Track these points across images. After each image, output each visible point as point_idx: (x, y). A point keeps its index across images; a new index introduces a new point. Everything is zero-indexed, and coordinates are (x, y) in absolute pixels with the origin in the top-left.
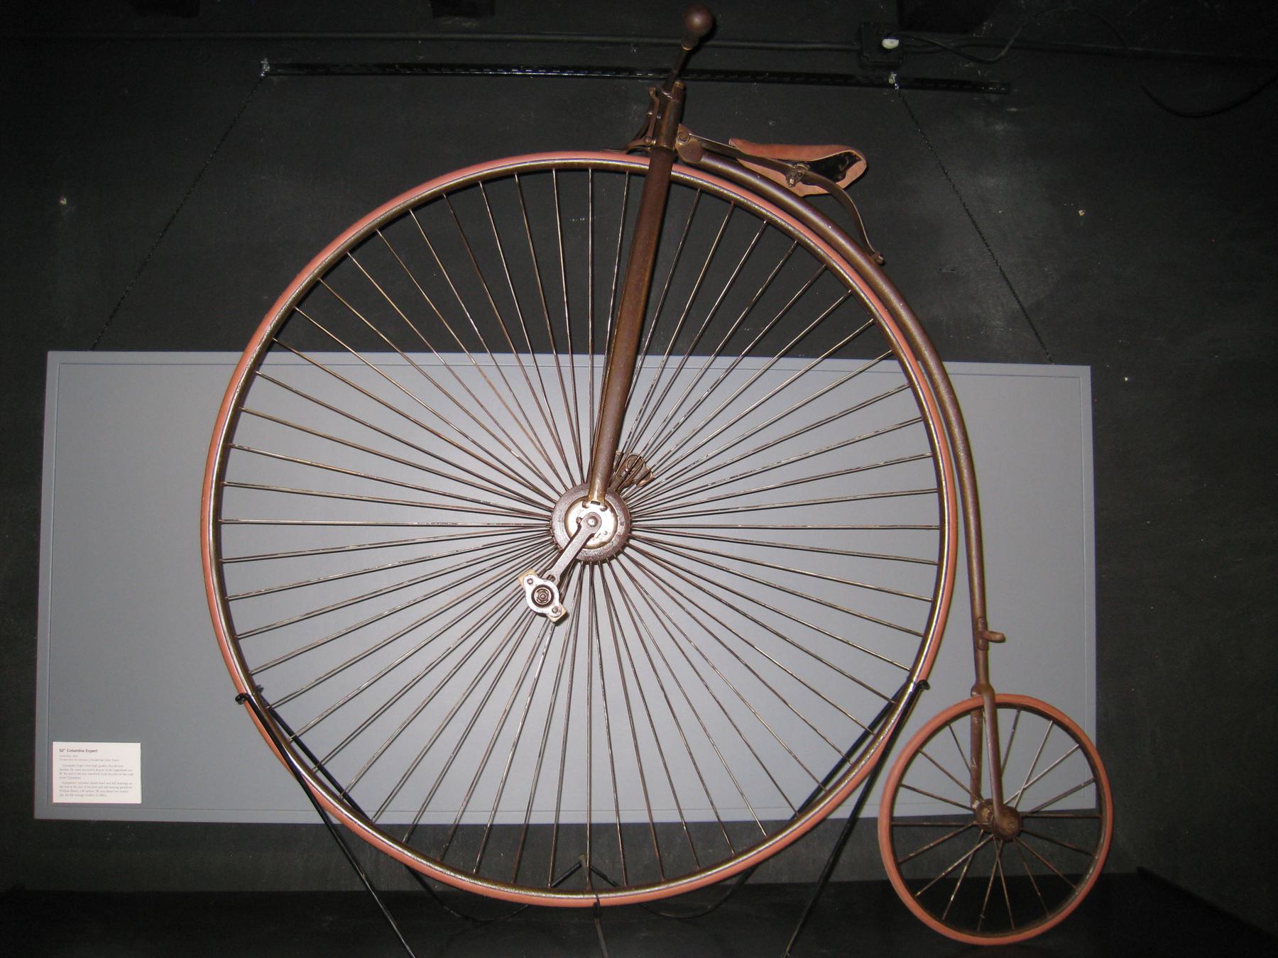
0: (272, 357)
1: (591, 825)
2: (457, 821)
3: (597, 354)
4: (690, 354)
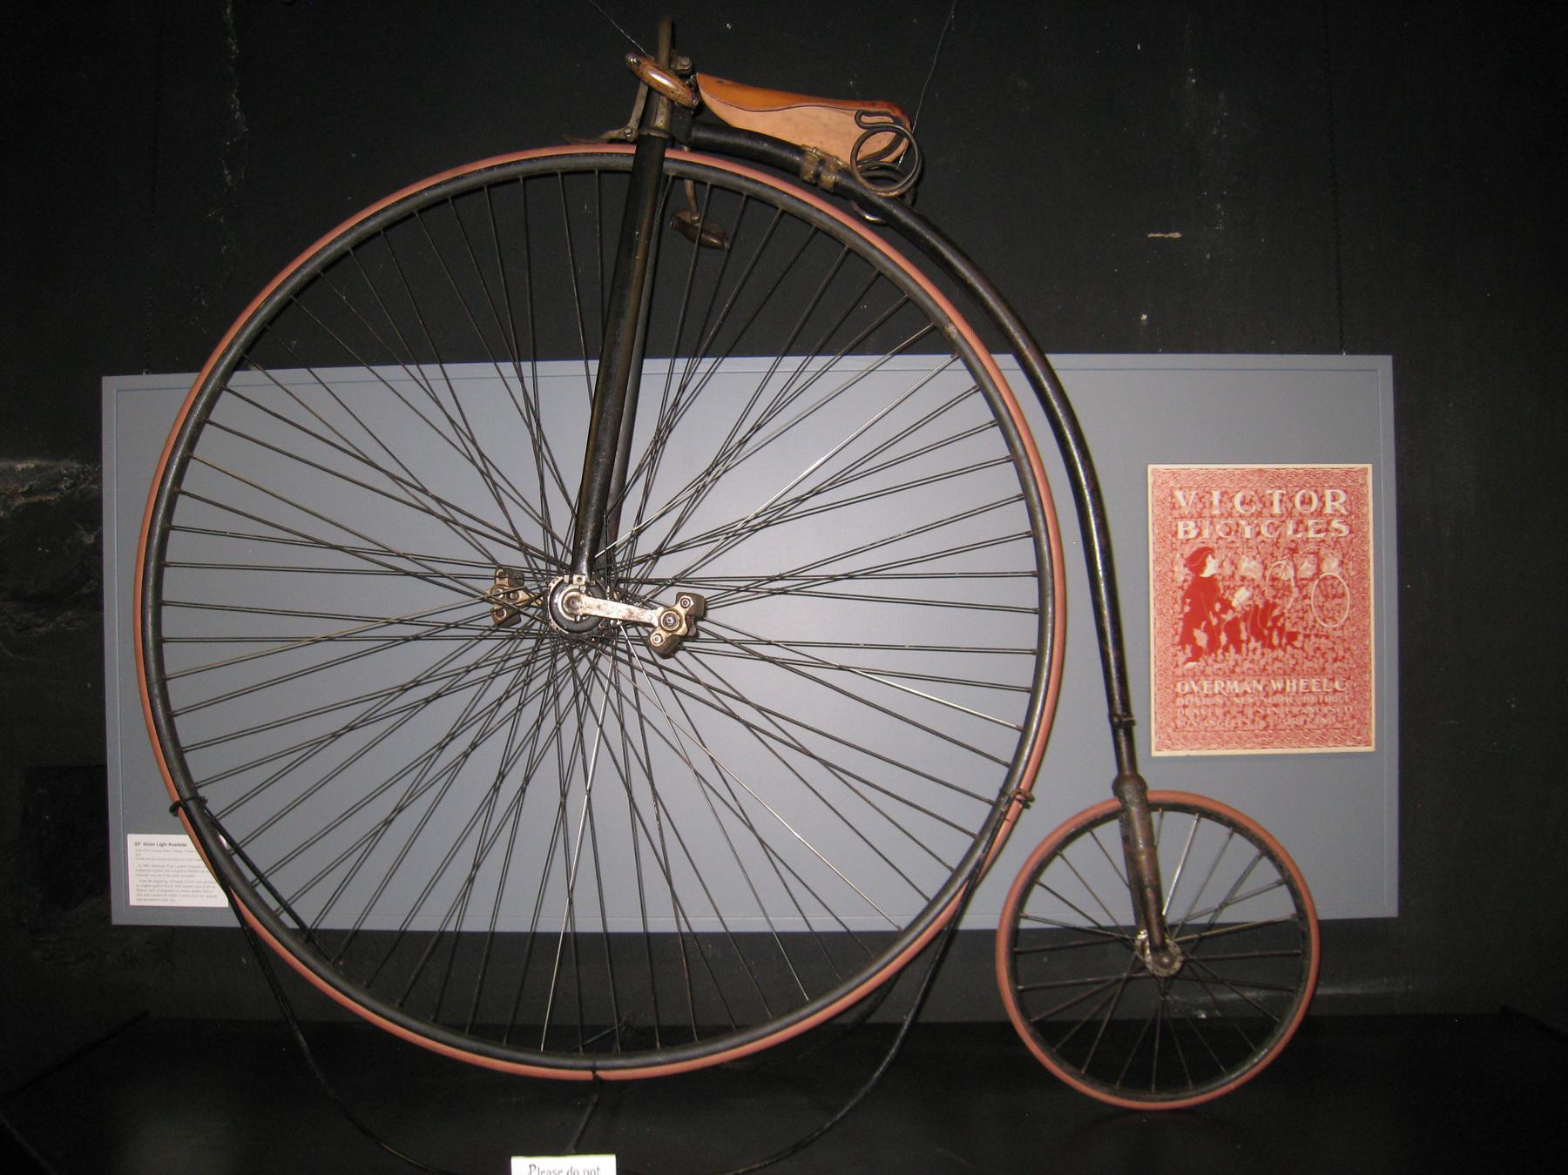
0: (239, 379)
1: (1016, 934)
2: (357, 926)
3: (524, 361)
4: (785, 354)
